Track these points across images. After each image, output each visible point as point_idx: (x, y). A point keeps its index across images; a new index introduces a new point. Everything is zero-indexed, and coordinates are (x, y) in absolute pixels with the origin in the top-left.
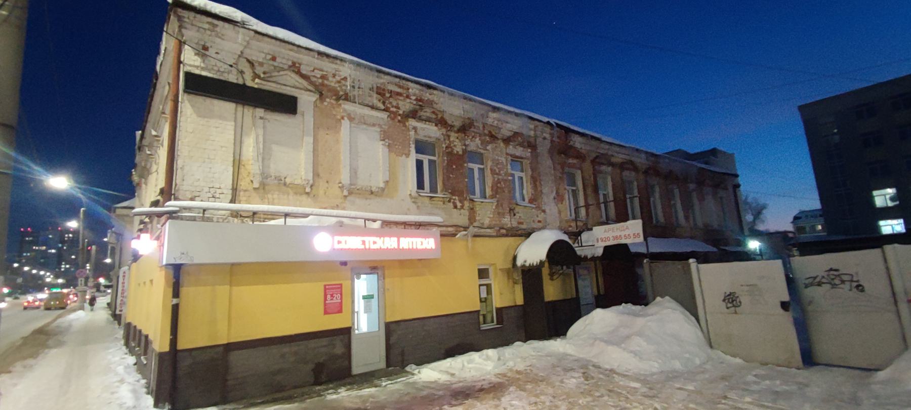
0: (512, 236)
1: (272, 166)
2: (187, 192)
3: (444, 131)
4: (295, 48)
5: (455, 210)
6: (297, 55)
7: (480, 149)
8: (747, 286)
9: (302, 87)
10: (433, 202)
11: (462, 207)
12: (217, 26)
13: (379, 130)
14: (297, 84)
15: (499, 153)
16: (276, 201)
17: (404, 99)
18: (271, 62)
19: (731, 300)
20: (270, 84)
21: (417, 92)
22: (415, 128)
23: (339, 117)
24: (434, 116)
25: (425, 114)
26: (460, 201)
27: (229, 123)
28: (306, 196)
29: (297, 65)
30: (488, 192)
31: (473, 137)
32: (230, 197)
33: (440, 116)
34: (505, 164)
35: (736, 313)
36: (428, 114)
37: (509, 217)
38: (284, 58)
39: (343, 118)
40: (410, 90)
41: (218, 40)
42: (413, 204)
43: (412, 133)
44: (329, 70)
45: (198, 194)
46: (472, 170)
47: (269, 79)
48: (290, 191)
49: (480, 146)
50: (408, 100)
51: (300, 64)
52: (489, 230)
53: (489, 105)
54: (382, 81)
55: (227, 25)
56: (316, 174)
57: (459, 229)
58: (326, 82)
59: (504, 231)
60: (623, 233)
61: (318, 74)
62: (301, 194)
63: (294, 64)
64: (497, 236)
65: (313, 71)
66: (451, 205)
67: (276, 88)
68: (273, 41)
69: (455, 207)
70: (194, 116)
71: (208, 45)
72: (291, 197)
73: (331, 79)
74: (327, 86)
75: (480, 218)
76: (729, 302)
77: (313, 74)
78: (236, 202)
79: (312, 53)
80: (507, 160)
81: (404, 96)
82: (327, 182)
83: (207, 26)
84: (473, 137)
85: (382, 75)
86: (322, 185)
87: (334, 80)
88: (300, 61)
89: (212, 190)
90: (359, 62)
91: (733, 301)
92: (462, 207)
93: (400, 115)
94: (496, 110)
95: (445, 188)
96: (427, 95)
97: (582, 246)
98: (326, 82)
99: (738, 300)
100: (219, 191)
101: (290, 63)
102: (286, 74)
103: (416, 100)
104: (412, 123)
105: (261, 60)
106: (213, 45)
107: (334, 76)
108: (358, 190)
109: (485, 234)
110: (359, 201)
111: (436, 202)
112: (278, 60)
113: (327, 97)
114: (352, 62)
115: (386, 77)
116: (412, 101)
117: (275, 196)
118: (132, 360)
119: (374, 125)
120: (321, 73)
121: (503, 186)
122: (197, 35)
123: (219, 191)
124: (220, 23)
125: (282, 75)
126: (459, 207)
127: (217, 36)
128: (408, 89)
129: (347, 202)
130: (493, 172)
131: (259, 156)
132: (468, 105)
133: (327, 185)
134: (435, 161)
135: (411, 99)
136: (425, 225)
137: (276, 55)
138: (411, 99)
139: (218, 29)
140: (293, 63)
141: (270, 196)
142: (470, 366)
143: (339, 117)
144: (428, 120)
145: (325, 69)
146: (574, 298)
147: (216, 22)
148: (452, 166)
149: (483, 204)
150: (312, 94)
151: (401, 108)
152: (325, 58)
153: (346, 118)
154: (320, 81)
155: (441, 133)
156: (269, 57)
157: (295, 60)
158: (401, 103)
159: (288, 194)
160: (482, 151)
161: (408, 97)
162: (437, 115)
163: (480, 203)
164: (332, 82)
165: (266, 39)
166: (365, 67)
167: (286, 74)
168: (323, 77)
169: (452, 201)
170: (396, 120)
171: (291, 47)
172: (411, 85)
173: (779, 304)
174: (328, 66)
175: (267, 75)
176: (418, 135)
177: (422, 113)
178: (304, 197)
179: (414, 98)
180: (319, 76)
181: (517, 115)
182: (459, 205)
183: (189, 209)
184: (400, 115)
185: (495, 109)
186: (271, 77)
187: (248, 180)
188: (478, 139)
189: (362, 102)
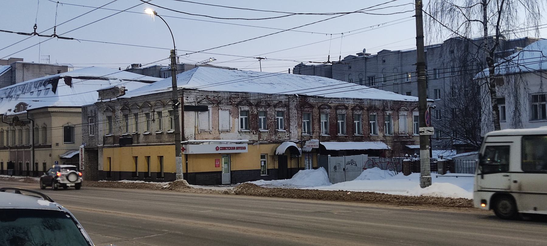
60: (314, 144)
69: (254, 134)
92: (256, 134)
123: (192, 135)
182: (255, 133)
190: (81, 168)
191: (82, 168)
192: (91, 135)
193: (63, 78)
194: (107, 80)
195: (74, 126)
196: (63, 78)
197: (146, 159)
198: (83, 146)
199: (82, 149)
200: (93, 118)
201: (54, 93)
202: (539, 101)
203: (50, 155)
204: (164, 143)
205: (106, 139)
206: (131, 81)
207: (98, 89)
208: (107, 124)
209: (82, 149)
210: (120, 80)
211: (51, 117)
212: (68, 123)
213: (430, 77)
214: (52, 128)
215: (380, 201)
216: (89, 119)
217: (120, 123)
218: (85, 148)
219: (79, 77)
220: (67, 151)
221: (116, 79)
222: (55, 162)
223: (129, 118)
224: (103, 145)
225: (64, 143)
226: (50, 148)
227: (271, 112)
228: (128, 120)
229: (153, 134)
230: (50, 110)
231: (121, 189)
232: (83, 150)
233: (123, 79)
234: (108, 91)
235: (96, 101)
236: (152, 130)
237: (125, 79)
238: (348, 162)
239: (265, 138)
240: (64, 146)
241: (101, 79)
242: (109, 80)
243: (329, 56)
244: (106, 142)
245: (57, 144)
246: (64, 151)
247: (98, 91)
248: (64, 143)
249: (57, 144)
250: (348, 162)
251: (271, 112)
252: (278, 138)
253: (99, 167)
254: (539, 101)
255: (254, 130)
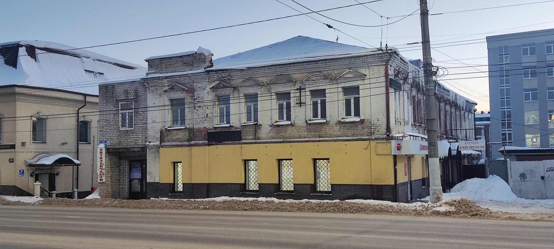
8: (530, 171)
19: (523, 176)
35: (524, 181)
60: (475, 145)
76: (522, 177)
91: (523, 176)
97: (466, 140)
99: (525, 176)
118: (166, 210)
136: (545, 227)
142: (428, 86)
146: (547, 126)
173: (540, 177)
190: (100, 180)
191: (102, 180)
192: (122, 129)
193: (24, 47)
194: (78, 57)
195: (45, 117)
196: (24, 47)
197: (243, 162)
198: (102, 146)
199: (101, 150)
200: (132, 102)
201: (11, 67)
203: (11, 161)
204: (329, 139)
205: (165, 134)
206: (105, 62)
207: (147, 58)
208: (170, 110)
209: (101, 150)
210: (93, 59)
211: (15, 101)
212: (38, 113)
213: (193, 106)
214: (230, 99)
215: (207, 210)
216: (120, 103)
217: (208, 108)
218: (106, 149)
219: (44, 48)
220: (37, 154)
221: (88, 58)
222: (20, 170)
223: (231, 102)
224: (161, 143)
225: (33, 143)
226: (13, 150)
228: (257, 101)
229: (296, 124)
230: (18, 90)
232: (104, 151)
233: (97, 59)
234: (174, 60)
235: (144, 76)
237: (99, 59)
238: (551, 168)
240: (31, 146)
241: (71, 56)
242: (80, 58)
243: (387, 45)
244: (166, 139)
245: (23, 144)
246: (33, 155)
247: (146, 61)
248: (33, 143)
249: (23, 144)
250: (551, 168)
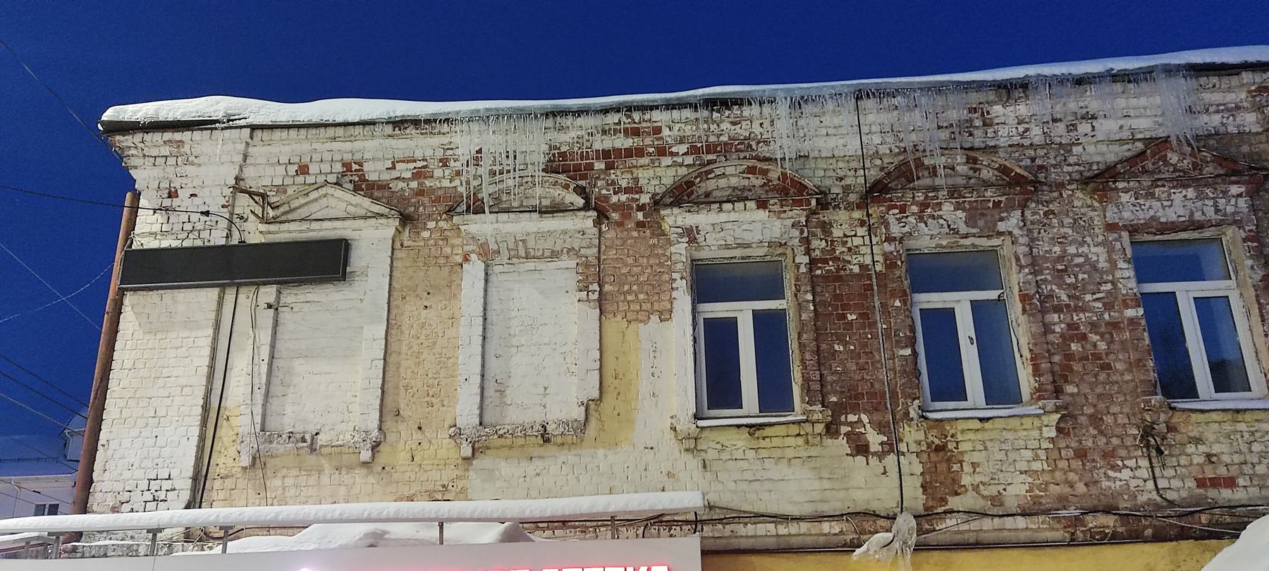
0: (1159, 537)
1: (289, 409)
2: (109, 495)
3: (799, 214)
4: (340, 131)
5: (860, 459)
6: (348, 146)
7: (966, 236)
9: (363, 212)
10: (763, 443)
11: (891, 447)
12: (180, 143)
13: (572, 264)
14: (351, 209)
15: (1070, 231)
16: (291, 492)
17: (653, 161)
18: (300, 179)
20: (285, 227)
21: (688, 130)
22: (691, 234)
23: (459, 259)
24: (757, 181)
25: (722, 183)
26: (881, 428)
27: (200, 333)
28: (364, 471)
29: (355, 167)
30: (1026, 380)
31: (924, 206)
32: (186, 495)
33: (774, 174)
34: (1103, 264)
36: (734, 181)
37: (1144, 463)
38: (1208, 88)
39: (466, 259)
40: (666, 132)
41: (189, 170)
42: (688, 457)
43: (680, 249)
44: (429, 153)
45: (126, 496)
46: (947, 316)
47: (290, 217)
48: (324, 461)
49: (963, 229)
50: (667, 161)
51: (360, 164)
52: (1021, 522)
53: (980, 86)
54: (573, 134)
55: (197, 135)
56: (387, 411)
57: (868, 526)
58: (428, 183)
59: (1108, 522)
61: (405, 170)
62: (350, 468)
63: (347, 166)
64: (1072, 543)
65: (394, 168)
66: (840, 445)
67: (301, 231)
68: (293, 132)
69: (861, 448)
70: (139, 334)
71: (176, 184)
72: (325, 480)
73: (438, 173)
74: (432, 190)
75: (978, 479)
77: (395, 174)
78: (203, 504)
79: (378, 128)
80: (1111, 251)
81: (650, 154)
82: (420, 428)
83: (165, 151)
84: (924, 206)
85: (568, 121)
86: (403, 439)
87: (447, 172)
88: (358, 157)
89: (153, 484)
90: (519, 109)
92: (891, 447)
93: (641, 208)
94: (1017, 93)
95: (817, 393)
96: (725, 127)
98: (428, 183)
100: (167, 485)
101: (338, 168)
102: (325, 196)
103: (693, 150)
104: (675, 218)
105: (278, 182)
106: (184, 180)
107: (444, 162)
108: (501, 436)
109: (809, 540)
110: (508, 469)
111: (776, 442)
112: (313, 169)
113: (430, 217)
114: (472, 118)
115: (580, 121)
116: (679, 160)
117: (289, 481)
119: (555, 255)
120: (412, 165)
121: (1102, 346)
122: (157, 172)
123: (167, 485)
124: (186, 136)
125: (316, 200)
126: (875, 447)
127: (187, 162)
128: (658, 130)
129: (471, 473)
130: (1038, 304)
131: (256, 390)
132: (875, 116)
133: (418, 436)
134: (780, 316)
135: (672, 154)
137: (306, 160)
138: (672, 154)
139: (186, 149)
140: (344, 165)
141: (277, 482)
143: (459, 259)
144: (739, 196)
145: (419, 155)
147: (178, 136)
148: (844, 317)
149: (987, 425)
150: (383, 221)
151: (645, 189)
152: (411, 130)
153: (473, 257)
154: (414, 184)
155: (789, 222)
156: (292, 169)
157: (348, 157)
158: (644, 175)
159: (320, 471)
160: (984, 243)
161: (662, 152)
162: (764, 172)
163: (977, 425)
164: (441, 180)
165: (278, 134)
166: (499, 115)
167: (325, 196)
168: (418, 175)
169: (844, 429)
170: (631, 225)
171: (331, 132)
172: (659, 116)
174: (422, 145)
175: (281, 210)
176: (699, 248)
177: (711, 185)
178: (359, 475)
179: (683, 149)
180: (408, 175)
181: (1146, 74)
182: (875, 439)
183: (108, 532)
184: (641, 208)
185: (1007, 90)
186: (291, 211)
187: (232, 452)
188: (947, 207)
189: (522, 205)
202: (47, 506)
227: (1062, 240)
231: (978, 79)
236: (265, 464)
239: (1017, 490)
251: (1062, 240)
252: (1201, 483)
253: (1111, 222)
254: (47, 506)
255: (855, 409)
